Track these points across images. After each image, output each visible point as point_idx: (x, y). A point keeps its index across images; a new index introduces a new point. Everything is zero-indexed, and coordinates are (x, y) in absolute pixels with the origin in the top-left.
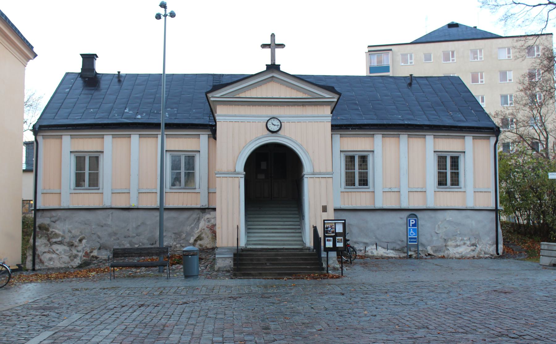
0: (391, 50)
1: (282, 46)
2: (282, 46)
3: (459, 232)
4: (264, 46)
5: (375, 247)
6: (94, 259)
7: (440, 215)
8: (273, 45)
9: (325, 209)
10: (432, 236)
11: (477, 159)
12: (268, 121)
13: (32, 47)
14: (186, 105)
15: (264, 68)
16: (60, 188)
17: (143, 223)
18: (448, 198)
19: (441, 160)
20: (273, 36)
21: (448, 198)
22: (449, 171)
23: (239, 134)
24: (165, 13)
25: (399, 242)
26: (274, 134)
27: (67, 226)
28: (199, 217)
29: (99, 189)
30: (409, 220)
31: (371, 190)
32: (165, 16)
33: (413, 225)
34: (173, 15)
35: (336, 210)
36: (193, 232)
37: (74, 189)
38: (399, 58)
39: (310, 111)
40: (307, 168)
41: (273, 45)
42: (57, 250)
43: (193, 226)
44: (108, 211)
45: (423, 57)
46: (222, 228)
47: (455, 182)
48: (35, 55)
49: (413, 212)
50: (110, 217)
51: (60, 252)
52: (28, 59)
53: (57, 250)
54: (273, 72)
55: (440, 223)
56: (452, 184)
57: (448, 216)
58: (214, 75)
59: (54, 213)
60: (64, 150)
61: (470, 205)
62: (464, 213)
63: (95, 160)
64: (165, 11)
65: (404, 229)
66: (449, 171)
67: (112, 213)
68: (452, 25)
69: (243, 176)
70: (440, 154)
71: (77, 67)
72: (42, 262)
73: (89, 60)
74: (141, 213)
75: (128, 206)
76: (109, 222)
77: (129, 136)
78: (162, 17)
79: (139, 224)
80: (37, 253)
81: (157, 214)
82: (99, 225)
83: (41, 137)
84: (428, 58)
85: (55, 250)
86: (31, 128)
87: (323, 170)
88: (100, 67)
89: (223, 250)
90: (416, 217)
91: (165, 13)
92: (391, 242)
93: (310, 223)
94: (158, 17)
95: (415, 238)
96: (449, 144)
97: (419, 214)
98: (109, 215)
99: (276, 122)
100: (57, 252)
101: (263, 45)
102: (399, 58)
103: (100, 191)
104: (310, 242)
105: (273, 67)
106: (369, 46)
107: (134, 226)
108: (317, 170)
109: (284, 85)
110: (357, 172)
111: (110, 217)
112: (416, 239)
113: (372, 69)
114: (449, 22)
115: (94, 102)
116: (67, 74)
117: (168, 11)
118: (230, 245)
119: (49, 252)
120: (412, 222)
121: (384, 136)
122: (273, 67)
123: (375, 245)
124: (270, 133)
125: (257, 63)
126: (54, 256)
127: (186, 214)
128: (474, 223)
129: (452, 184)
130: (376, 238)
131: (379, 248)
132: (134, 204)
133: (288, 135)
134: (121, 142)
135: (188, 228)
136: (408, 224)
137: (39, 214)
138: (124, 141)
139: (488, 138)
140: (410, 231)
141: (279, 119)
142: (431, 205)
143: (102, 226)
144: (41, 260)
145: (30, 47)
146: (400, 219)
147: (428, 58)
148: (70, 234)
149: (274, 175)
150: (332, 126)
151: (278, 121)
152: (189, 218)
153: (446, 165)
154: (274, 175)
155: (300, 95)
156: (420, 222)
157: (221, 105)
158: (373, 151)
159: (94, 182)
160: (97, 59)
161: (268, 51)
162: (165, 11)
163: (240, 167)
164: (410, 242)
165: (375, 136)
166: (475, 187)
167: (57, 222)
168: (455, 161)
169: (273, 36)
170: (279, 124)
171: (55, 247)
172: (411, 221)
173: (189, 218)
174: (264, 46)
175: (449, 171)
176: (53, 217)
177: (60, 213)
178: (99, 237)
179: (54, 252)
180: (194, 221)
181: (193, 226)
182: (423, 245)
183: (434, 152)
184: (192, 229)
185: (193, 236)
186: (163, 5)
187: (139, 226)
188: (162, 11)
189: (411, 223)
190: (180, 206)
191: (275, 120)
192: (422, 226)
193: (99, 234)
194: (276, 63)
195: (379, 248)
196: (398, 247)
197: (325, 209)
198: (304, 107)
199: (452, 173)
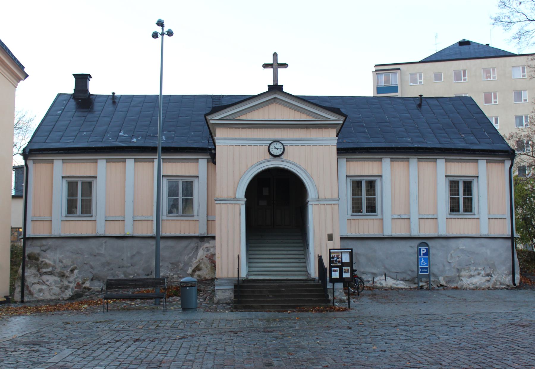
0: (399, 69)
1: (285, 66)
2: (285, 66)
3: (472, 262)
4: (266, 66)
5: (383, 277)
6: (87, 290)
7: (453, 243)
8: (275, 65)
9: (330, 238)
10: (444, 266)
11: (491, 183)
12: (270, 144)
13: (23, 67)
14: (185, 127)
15: (266, 89)
16: (52, 217)
17: (138, 253)
18: (462, 226)
19: (453, 185)
20: (275, 55)
21: (462, 226)
22: (461, 197)
23: (240, 158)
24: (162, 31)
25: (410, 273)
26: (277, 159)
27: (58, 255)
28: (197, 247)
29: (92, 216)
30: (420, 249)
31: (379, 217)
32: (163, 34)
33: (425, 254)
34: (170, 33)
35: (342, 238)
36: (191, 262)
37: (66, 217)
38: (408, 78)
39: (314, 134)
40: (312, 194)
41: (275, 65)
42: (48, 281)
43: (191, 255)
44: (101, 239)
45: (433, 76)
46: (221, 257)
47: (469, 208)
48: (26, 76)
49: (424, 241)
50: (104, 246)
51: (51, 283)
52: (19, 79)
53: (48, 281)
54: (275, 93)
55: (452, 252)
56: (465, 211)
57: (462, 244)
58: (213, 96)
59: (44, 242)
60: (57, 173)
61: (485, 232)
62: (478, 241)
63: (88, 185)
64: (163, 29)
65: (414, 258)
66: (461, 198)
67: (106, 242)
68: (464, 43)
69: (244, 203)
70: (452, 179)
71: (69, 88)
72: (31, 293)
73: (82, 80)
74: (136, 241)
75: (122, 234)
76: (103, 252)
77: (124, 161)
78: (159, 35)
79: (134, 253)
80: (26, 284)
81: (153, 242)
82: (91, 255)
83: (32, 161)
84: (438, 77)
85: (45, 281)
86: (21, 151)
87: (328, 196)
88: (95, 88)
89: (223, 282)
90: (427, 245)
91: (162, 31)
92: (401, 273)
93: (315, 253)
94: (155, 35)
95: (427, 268)
96: (462, 169)
97: (431, 243)
98: (102, 244)
99: (278, 146)
100: (48, 283)
101: (277, 55)
102: (408, 78)
103: (93, 219)
104: (315, 273)
105: (275, 88)
106: (376, 66)
107: (129, 255)
108: (322, 197)
109: (287, 106)
110: (364, 197)
111: (104, 246)
112: (428, 269)
113: (379, 90)
114: (460, 39)
115: (87, 124)
116: (59, 95)
117: (166, 29)
118: (230, 276)
119: (39, 283)
120: (423, 250)
121: (392, 160)
122: (275, 88)
123: (384, 276)
124: (272, 157)
125: (258, 83)
126: (44, 287)
127: (184, 243)
128: (488, 252)
129: (465, 211)
130: (385, 268)
131: (388, 279)
132: (128, 232)
133: (291, 159)
134: (116, 167)
135: (186, 258)
136: (418, 252)
137: (28, 243)
138: (119, 165)
139: (503, 162)
140: (421, 260)
141: (282, 142)
142: (443, 232)
143: (95, 256)
144: (30, 291)
145: (21, 68)
146: (410, 248)
147: (438, 77)
148: (61, 264)
149: (276, 202)
150: (338, 149)
151: (280, 145)
152: (186, 247)
153: (458, 191)
154: (276, 202)
155: (304, 117)
156: (432, 251)
157: (220, 127)
158: (381, 176)
159: (87, 209)
160: (91, 79)
161: (270, 71)
162: (163, 29)
163: (241, 193)
164: (421, 272)
165: (384, 160)
166: (489, 213)
167: (48, 251)
168: (468, 187)
169: (275, 55)
170: (282, 147)
171: (45, 278)
172: (422, 249)
173: (186, 247)
174: (266, 66)
175: (461, 197)
176: (43, 246)
177: (50, 242)
178: (92, 268)
179: (44, 283)
180: (193, 250)
181: (191, 255)
182: (435, 276)
183: (446, 176)
184: (190, 258)
185: (191, 266)
186: (160, 24)
187: (134, 255)
188: (159, 29)
189: (422, 252)
190: (178, 234)
191: (278, 143)
192: (434, 255)
193: (92, 263)
194: (279, 84)
195: (388, 279)
196: (408, 278)
197: (330, 238)
198: (309, 130)
199: (464, 199)
